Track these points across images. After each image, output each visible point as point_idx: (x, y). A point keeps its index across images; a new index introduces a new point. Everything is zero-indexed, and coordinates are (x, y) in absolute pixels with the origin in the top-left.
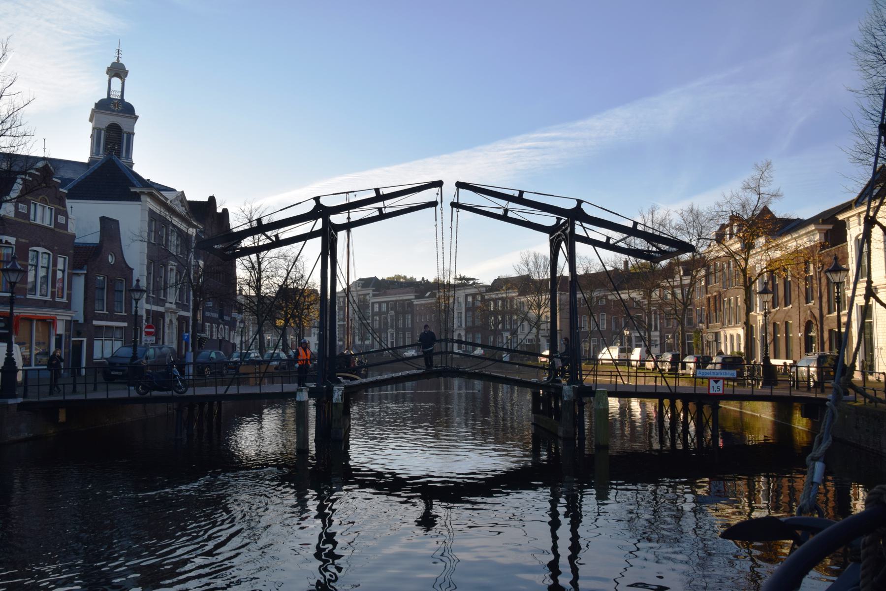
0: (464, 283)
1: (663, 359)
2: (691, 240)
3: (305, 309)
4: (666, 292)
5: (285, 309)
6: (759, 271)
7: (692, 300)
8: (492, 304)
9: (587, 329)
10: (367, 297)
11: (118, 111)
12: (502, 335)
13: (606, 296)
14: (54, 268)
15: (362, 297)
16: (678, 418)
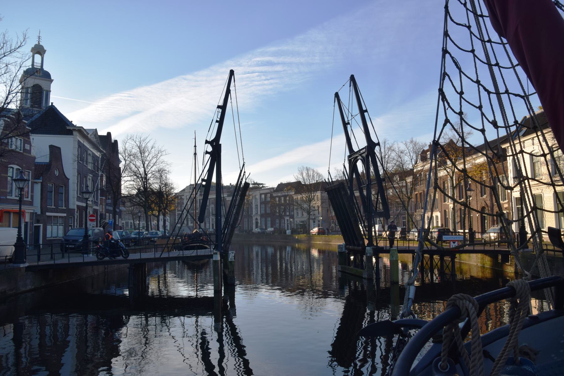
11: (40, 77)
12: (284, 218)
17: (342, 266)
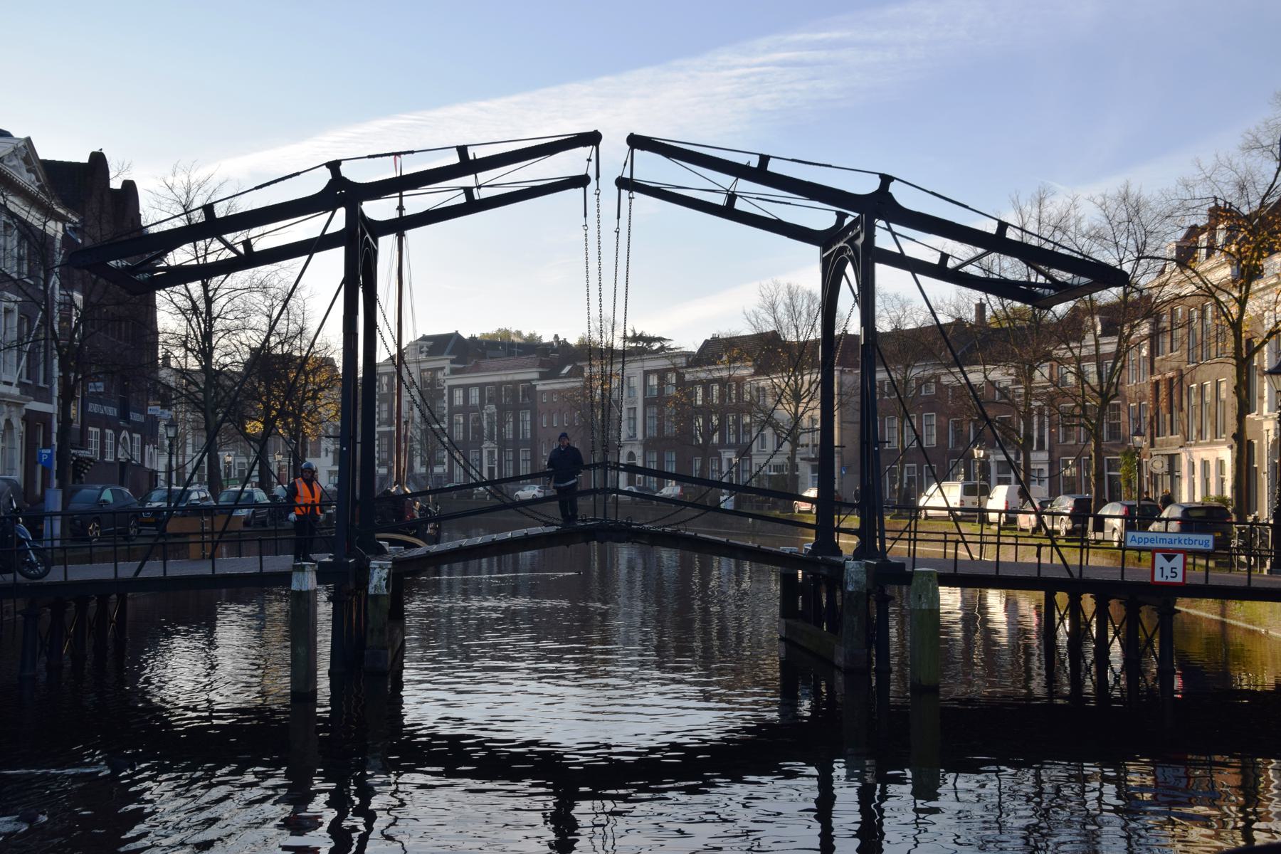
0: (642, 346)
1: (1056, 509)
2: (1121, 261)
3: (309, 398)
4: (1064, 371)
5: (264, 398)
6: (1270, 326)
7: (1120, 387)
8: (700, 391)
9: (895, 445)
10: (440, 375)
12: (719, 455)
13: (937, 377)
15: (427, 375)
16: (1085, 633)
17: (788, 621)
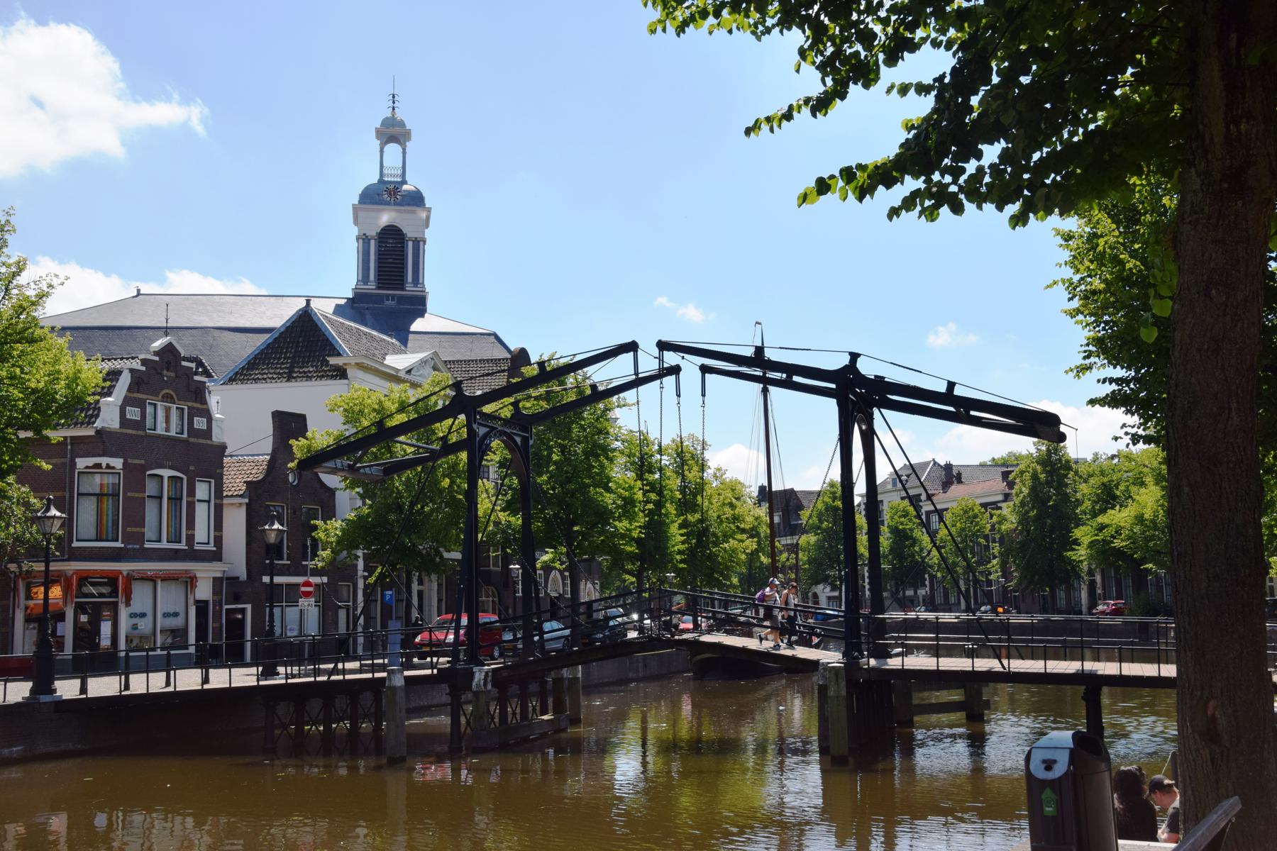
14: (190, 499)
